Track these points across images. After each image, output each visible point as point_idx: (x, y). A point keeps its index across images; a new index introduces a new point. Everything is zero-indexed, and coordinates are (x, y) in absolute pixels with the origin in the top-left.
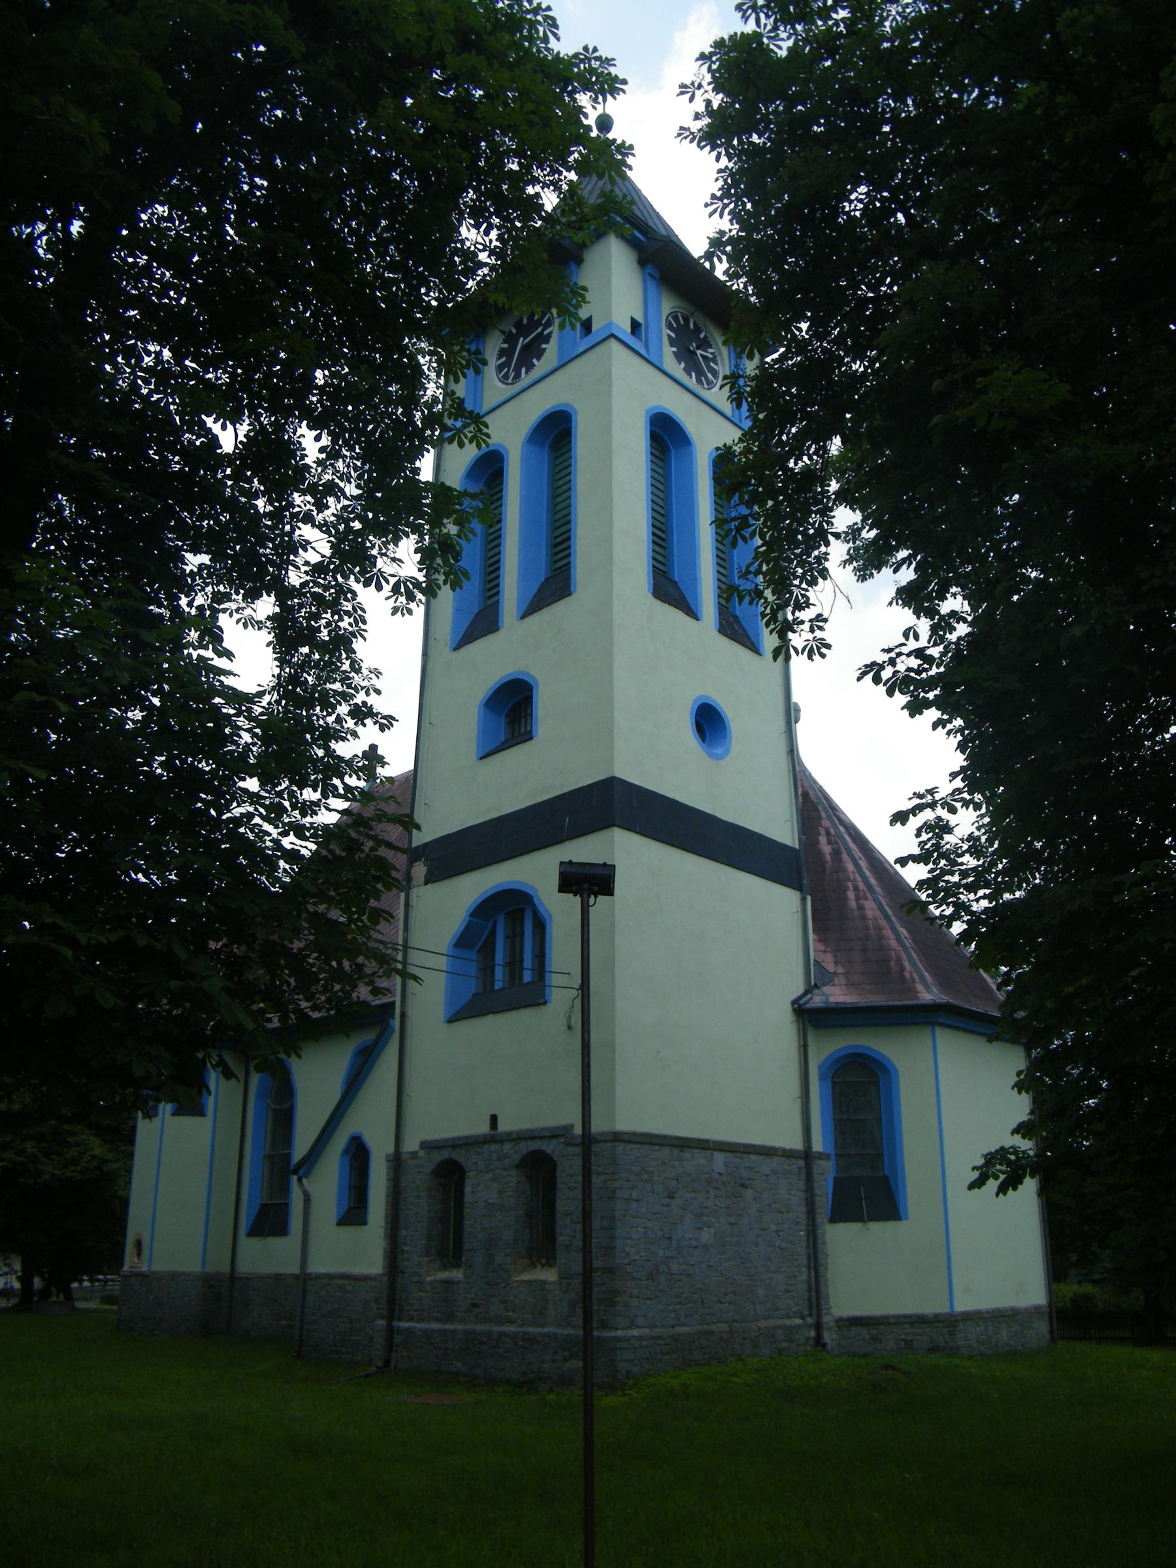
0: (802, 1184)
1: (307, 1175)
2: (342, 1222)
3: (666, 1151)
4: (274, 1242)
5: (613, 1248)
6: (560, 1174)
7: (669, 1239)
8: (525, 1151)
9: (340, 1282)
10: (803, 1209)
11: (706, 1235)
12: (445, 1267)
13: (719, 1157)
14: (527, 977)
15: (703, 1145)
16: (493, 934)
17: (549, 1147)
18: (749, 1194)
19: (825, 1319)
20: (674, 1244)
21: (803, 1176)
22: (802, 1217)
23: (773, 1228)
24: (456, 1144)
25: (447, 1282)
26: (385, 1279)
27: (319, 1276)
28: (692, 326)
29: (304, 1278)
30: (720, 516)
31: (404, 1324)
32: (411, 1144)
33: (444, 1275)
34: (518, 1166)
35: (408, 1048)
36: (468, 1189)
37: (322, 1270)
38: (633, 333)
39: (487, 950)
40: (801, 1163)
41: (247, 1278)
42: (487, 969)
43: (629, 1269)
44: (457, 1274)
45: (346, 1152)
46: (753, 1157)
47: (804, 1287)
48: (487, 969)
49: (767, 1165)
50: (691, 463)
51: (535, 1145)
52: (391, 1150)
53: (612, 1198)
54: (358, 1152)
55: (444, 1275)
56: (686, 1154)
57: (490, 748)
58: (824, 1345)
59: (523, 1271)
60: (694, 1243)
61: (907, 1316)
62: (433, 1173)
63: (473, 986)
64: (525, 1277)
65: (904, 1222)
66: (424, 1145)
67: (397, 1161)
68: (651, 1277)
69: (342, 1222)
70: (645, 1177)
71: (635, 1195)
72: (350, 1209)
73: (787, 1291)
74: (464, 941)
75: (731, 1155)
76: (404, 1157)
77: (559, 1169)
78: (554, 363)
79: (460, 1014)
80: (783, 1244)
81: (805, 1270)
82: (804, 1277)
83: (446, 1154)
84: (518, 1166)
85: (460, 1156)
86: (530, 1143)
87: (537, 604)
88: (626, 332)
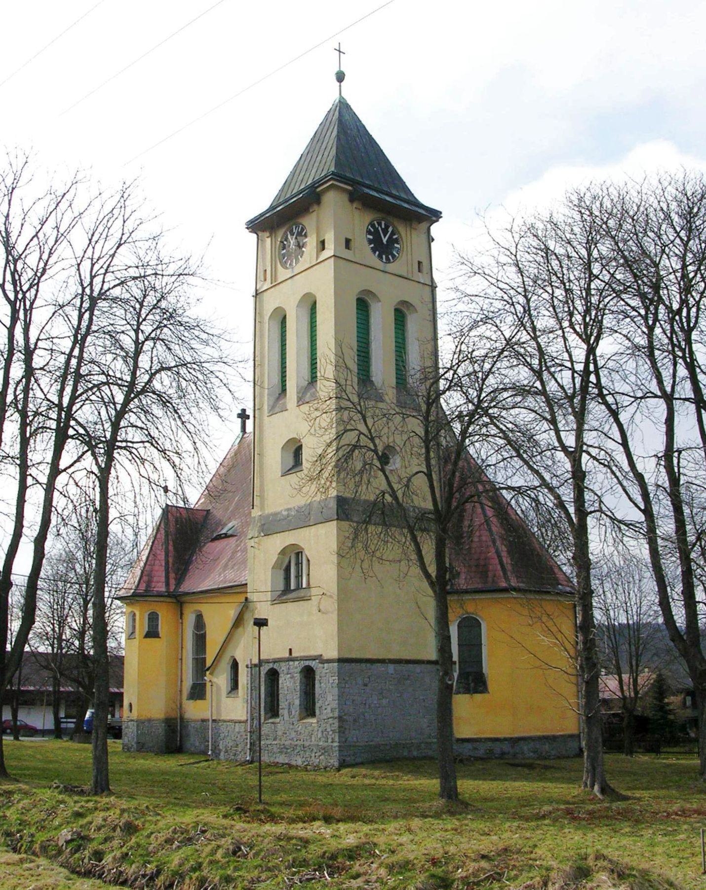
3: (363, 665)
13: (391, 668)
15: (382, 661)
17: (312, 664)
20: (367, 706)
39: (287, 570)
49: (418, 668)
51: (307, 663)
63: (281, 587)
83: (271, 665)
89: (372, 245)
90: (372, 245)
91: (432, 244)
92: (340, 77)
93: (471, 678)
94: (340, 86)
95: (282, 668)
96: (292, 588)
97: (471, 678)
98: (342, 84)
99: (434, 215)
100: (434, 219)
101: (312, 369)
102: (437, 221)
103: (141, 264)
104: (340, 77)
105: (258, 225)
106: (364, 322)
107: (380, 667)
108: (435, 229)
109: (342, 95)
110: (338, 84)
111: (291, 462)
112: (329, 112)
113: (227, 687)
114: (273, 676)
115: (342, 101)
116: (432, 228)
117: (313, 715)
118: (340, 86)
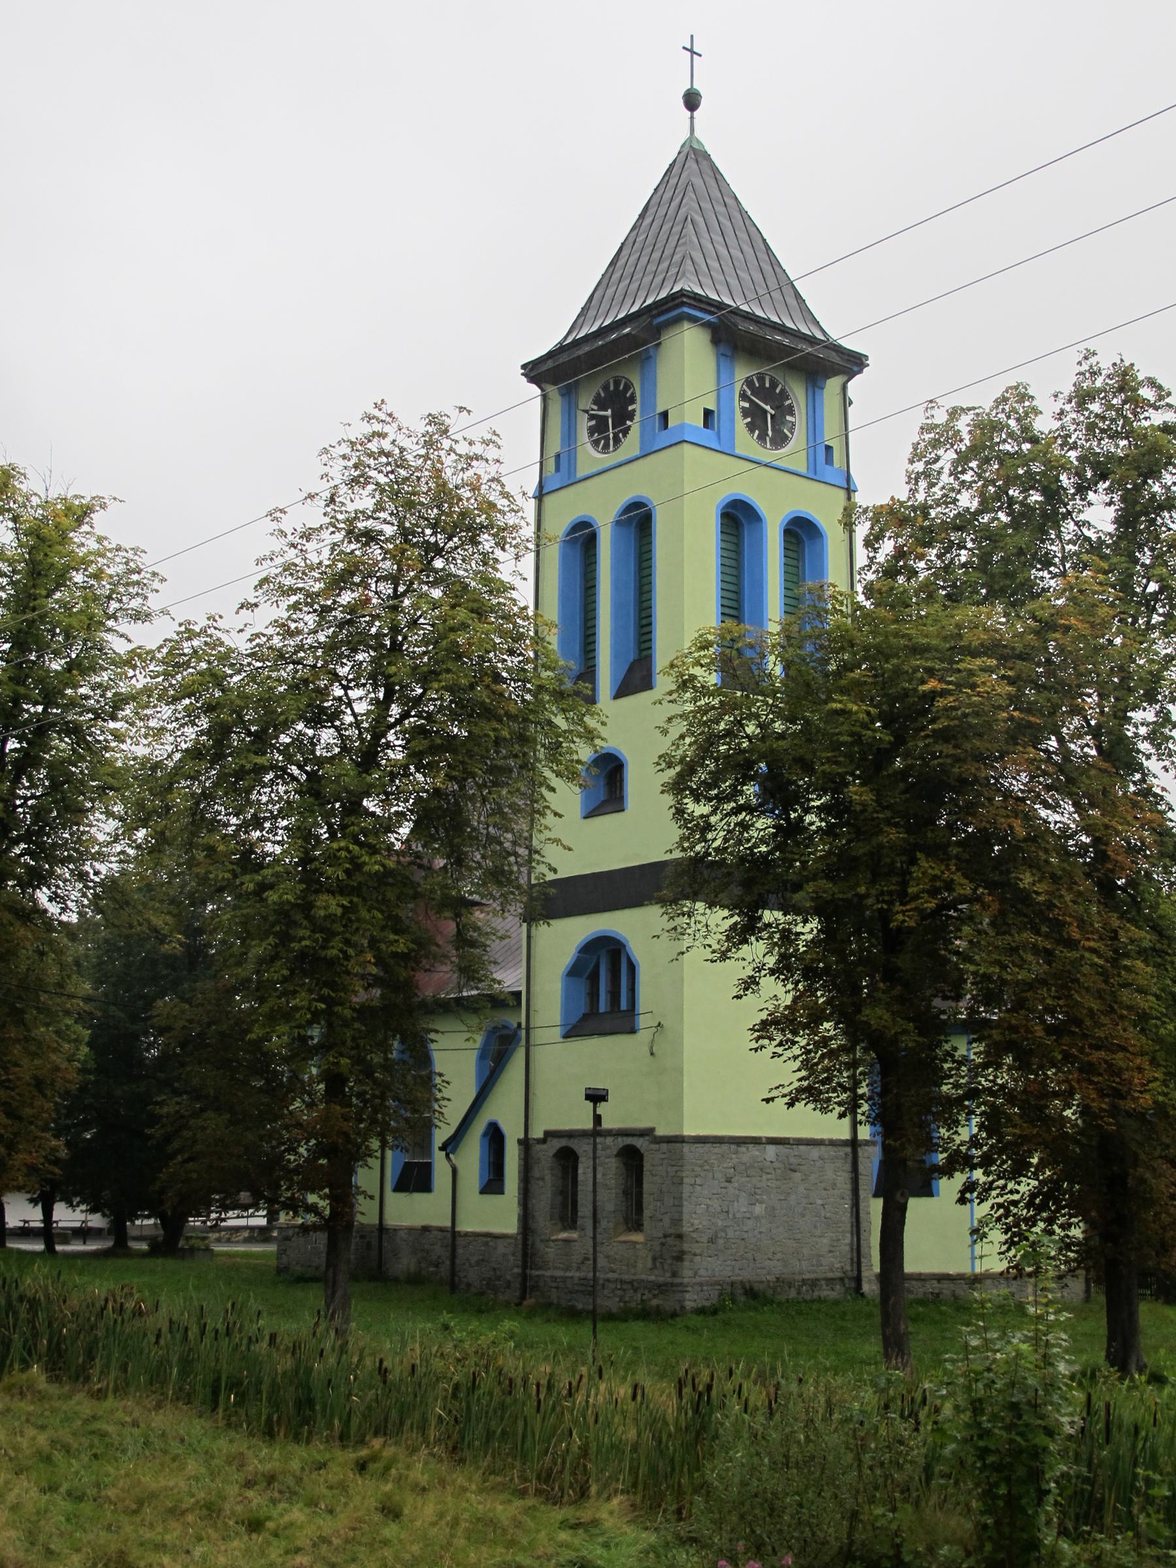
0: (848, 1167)
1: (453, 1152)
2: (483, 1191)
3: (725, 1147)
4: (419, 1199)
5: (681, 1220)
6: (647, 1166)
7: (727, 1212)
8: (621, 1145)
9: (485, 1239)
10: (849, 1186)
11: (759, 1209)
12: (564, 1229)
13: (771, 1150)
14: (624, 1005)
15: (756, 1141)
16: (597, 966)
17: (639, 1143)
18: (797, 1176)
19: (865, 1274)
20: (731, 1216)
21: (850, 1159)
22: (848, 1194)
23: (820, 1202)
24: (570, 1134)
25: (567, 1241)
26: (520, 1237)
27: (467, 1234)
28: (767, 385)
29: (452, 1235)
30: (790, 594)
31: (535, 1273)
32: (537, 1133)
33: (564, 1235)
34: (617, 1156)
35: (531, 1058)
36: (580, 1171)
37: (469, 1229)
38: (706, 425)
39: (594, 978)
40: (849, 1150)
41: (395, 1230)
42: (593, 996)
43: (694, 1235)
44: (574, 1235)
45: (485, 1135)
46: (802, 1148)
47: (848, 1248)
48: (593, 996)
49: (815, 1152)
50: (761, 546)
51: (629, 1141)
52: (522, 1136)
53: (681, 1183)
54: (495, 1136)
55: (564, 1235)
56: (743, 1149)
57: (592, 808)
58: (862, 1295)
59: (620, 1234)
60: (748, 1215)
61: (934, 1275)
62: (555, 1155)
63: (583, 1007)
64: (623, 1238)
65: (935, 1199)
66: (549, 1134)
67: (525, 1144)
68: (712, 1241)
69: (483, 1191)
70: (707, 1167)
71: (698, 1182)
72: (490, 1180)
73: (830, 1251)
74: (574, 972)
75: (780, 1147)
76: (531, 1142)
77: (645, 1159)
78: (637, 452)
79: (573, 1031)
80: (828, 1215)
81: (849, 1235)
82: (848, 1241)
83: (564, 1142)
84: (617, 1156)
85: (573, 1144)
86: (625, 1138)
87: (623, 690)
88: (697, 428)
89: (749, 420)
90: (749, 420)
91: (850, 410)
92: (692, 101)
93: (885, 907)
94: (692, 118)
95: (583, 1148)
96: (602, 1009)
97: (885, 907)
98: (696, 113)
99: (854, 363)
100: (856, 369)
101: (640, 643)
102: (860, 372)
103: (167, 1458)
104: (692, 101)
105: (536, 372)
106: (734, 604)
107: (754, 1151)
108: (855, 386)
109: (697, 134)
110: (688, 113)
111: (602, 796)
112: (672, 166)
113: (481, 1176)
114: (567, 1159)
115: (695, 146)
116: (851, 385)
117: (638, 1226)
118: (692, 118)
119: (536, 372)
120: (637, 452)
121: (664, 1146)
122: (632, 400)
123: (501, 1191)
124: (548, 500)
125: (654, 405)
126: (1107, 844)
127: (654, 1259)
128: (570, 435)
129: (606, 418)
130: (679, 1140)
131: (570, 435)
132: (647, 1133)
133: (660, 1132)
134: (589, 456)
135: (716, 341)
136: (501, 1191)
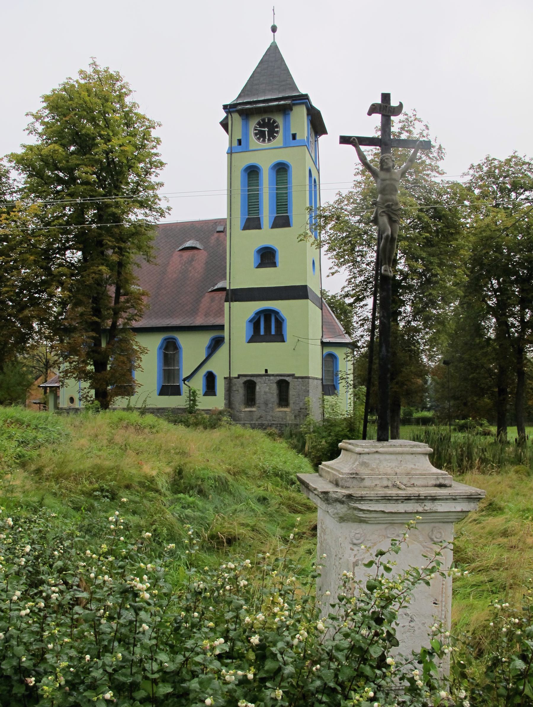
32: (234, 375)
66: (239, 376)
67: (229, 380)
92: (274, 29)
104: (274, 29)
105: (225, 107)
117: (287, 405)
119: (225, 107)
120: (282, 145)
121: (300, 380)
122: (277, 127)
123: (214, 394)
124: (233, 155)
125: (289, 130)
126: (93, 308)
127: (295, 416)
128: (246, 134)
129: (265, 131)
130: (308, 378)
131: (246, 134)
132: (293, 375)
133: (297, 375)
134: (254, 142)
135: (240, 115)
136: (214, 394)
